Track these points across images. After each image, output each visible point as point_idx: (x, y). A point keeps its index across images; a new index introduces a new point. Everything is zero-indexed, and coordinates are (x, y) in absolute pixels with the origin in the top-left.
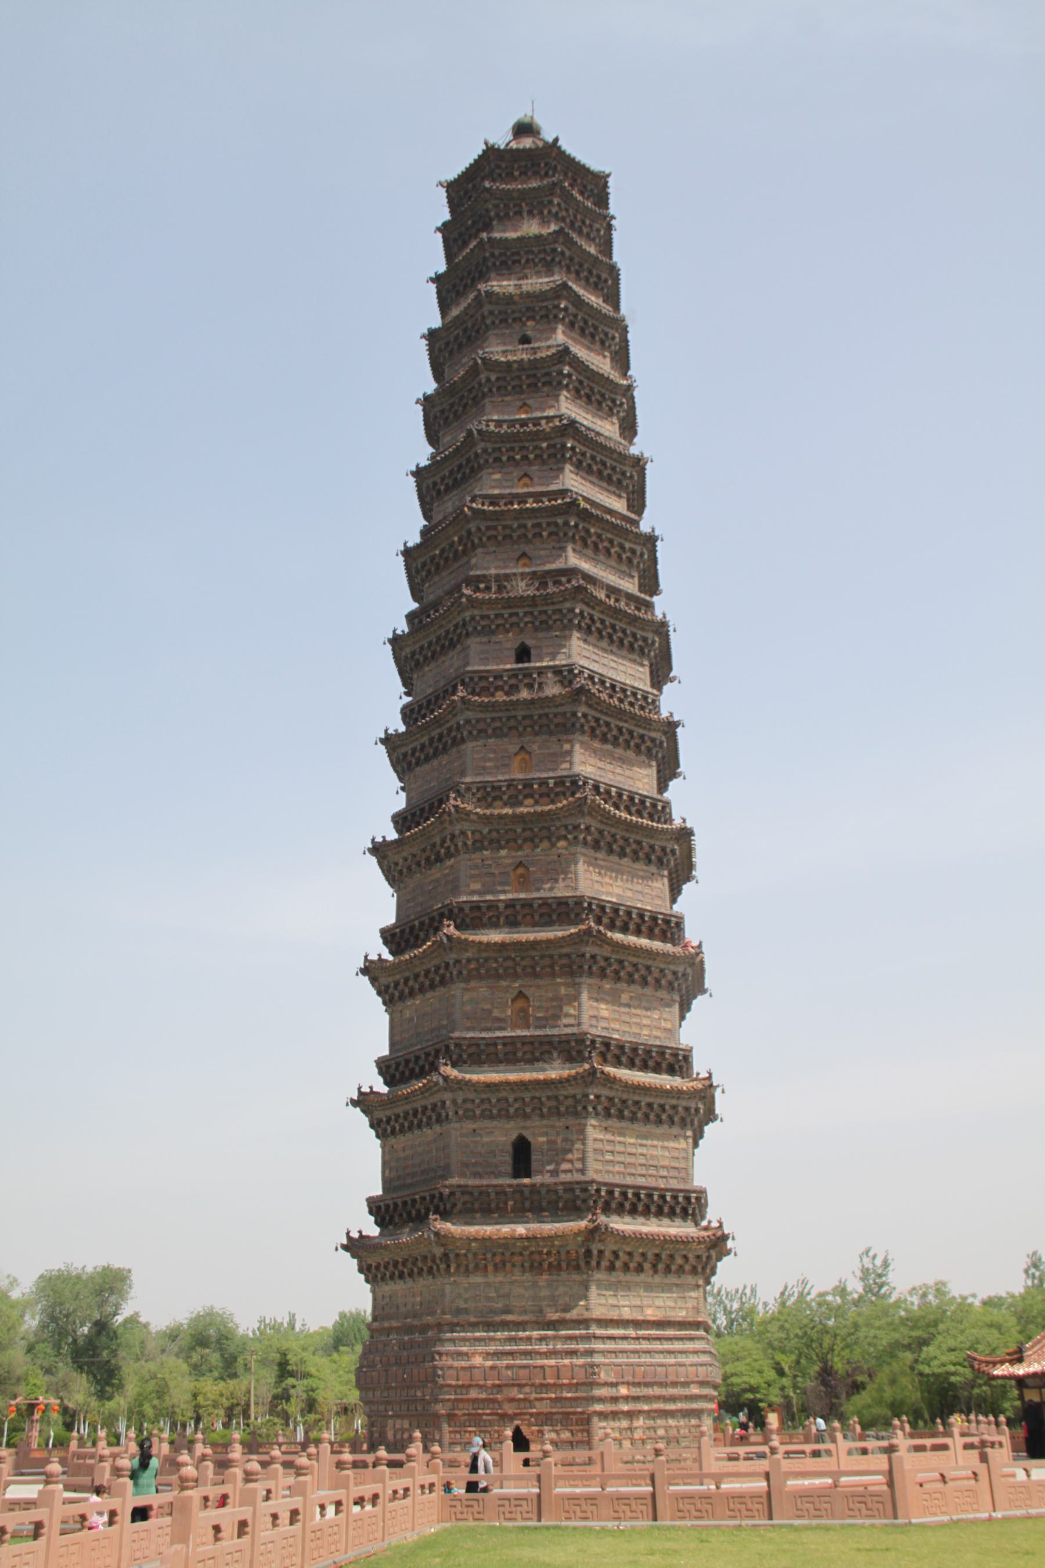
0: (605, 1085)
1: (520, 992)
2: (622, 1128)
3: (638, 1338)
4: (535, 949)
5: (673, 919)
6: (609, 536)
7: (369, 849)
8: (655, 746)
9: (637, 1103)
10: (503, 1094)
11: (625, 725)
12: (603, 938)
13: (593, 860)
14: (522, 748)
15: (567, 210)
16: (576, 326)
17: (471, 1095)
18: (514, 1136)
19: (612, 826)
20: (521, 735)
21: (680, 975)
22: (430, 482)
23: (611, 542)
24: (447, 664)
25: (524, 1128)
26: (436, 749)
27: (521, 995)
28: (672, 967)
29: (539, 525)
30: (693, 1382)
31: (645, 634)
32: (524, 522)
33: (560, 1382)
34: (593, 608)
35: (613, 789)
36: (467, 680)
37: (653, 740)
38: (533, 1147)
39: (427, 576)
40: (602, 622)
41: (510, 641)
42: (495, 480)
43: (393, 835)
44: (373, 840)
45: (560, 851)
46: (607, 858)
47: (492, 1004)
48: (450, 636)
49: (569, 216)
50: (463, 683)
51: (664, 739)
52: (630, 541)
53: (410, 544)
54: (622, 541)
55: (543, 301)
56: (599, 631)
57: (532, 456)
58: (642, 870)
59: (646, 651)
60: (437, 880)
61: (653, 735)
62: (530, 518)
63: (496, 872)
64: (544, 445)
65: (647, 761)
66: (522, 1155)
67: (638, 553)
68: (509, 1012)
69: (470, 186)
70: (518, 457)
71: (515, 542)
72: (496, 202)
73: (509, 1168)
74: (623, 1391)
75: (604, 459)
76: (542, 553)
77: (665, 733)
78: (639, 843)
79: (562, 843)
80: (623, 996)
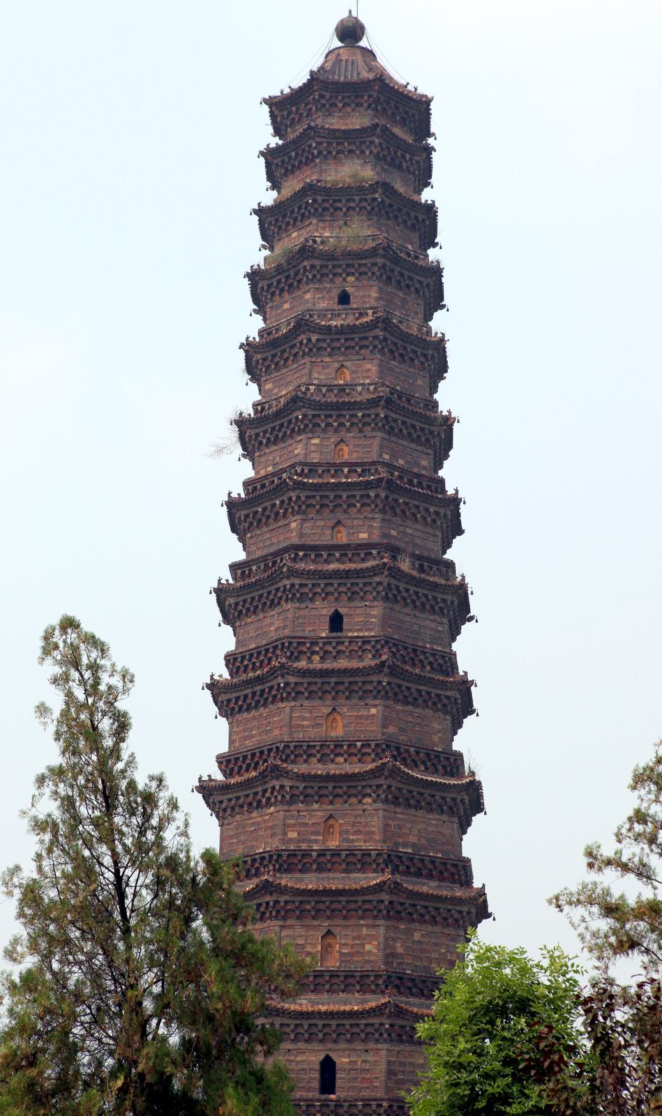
0: (398, 1016)
1: (329, 930)
2: (412, 1051)
5: (460, 863)
6: (416, 503)
7: (196, 787)
8: (451, 703)
11: (425, 688)
12: (400, 887)
13: (393, 815)
14: (334, 709)
15: (388, 148)
16: (393, 280)
17: (286, 1021)
18: (322, 1057)
19: (409, 784)
21: (429, 357)
22: (253, 432)
23: (417, 507)
24: (268, 620)
25: (330, 1050)
28: (458, 908)
31: (445, 597)
32: (340, 493)
34: (399, 580)
35: (412, 749)
37: (448, 698)
38: (337, 1067)
39: (249, 528)
40: (407, 590)
41: (324, 609)
42: (314, 444)
43: (219, 776)
44: (200, 779)
45: (365, 807)
46: (406, 811)
47: (306, 940)
49: (390, 153)
51: (458, 696)
52: (435, 505)
53: (271, 146)
54: (427, 506)
55: (362, 259)
56: (404, 599)
58: (436, 819)
59: (446, 611)
60: (258, 823)
61: (449, 693)
62: (344, 490)
63: (310, 822)
65: (443, 716)
66: (336, 622)
67: (442, 515)
68: (319, 948)
69: (294, 109)
72: (319, 140)
73: (316, 1084)
75: (414, 422)
76: (355, 522)
77: (460, 691)
79: (368, 800)
80: (416, 934)
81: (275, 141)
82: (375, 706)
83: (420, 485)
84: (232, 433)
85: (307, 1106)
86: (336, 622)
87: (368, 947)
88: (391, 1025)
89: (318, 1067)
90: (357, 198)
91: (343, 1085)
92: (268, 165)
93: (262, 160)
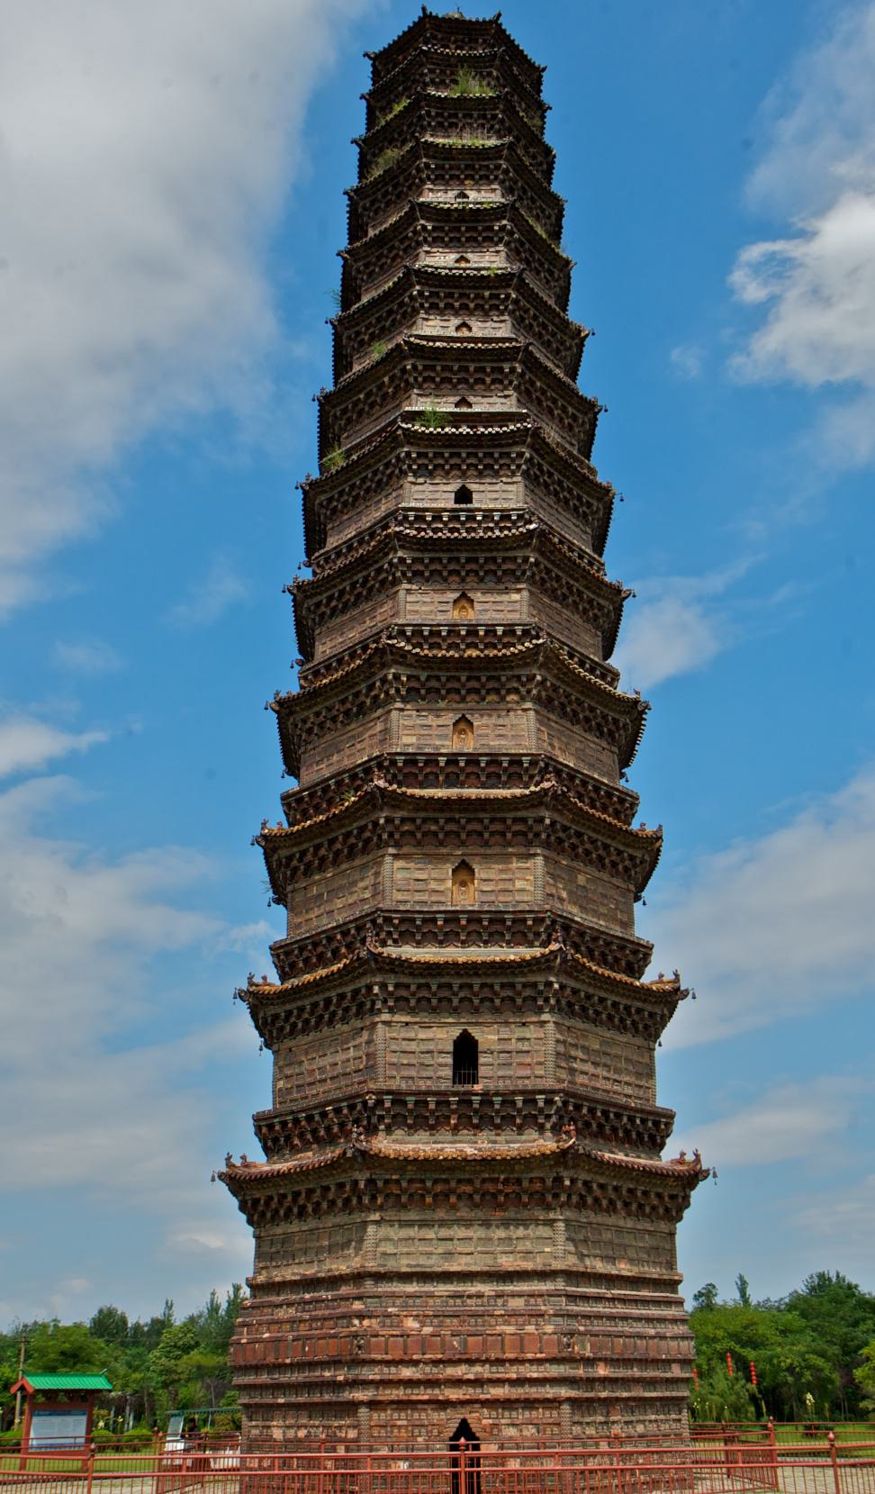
3: (613, 1299)
4: (485, 810)
9: (602, 1000)
10: (446, 980)
20: (463, 580)
23: (593, 842)
26: (359, 596)
27: (464, 1429)
29: (483, 370)
30: (674, 1361)
33: (522, 1356)
36: (380, 921)
38: (480, 1048)
43: (259, 1159)
48: (353, 840)
50: (380, 766)
57: (472, 305)
64: (487, 294)
70: (457, 304)
71: (455, 386)
74: (602, 1371)
78: (592, 710)
81: (307, 575)
82: (519, 591)
83: (592, 671)
84: (256, 864)
85: (438, 1103)
86: (466, 1052)
87: (519, 884)
88: (562, 987)
89: (450, 1048)
90: (475, 114)
91: (490, 1074)
92: (297, 606)
93: (364, 103)
